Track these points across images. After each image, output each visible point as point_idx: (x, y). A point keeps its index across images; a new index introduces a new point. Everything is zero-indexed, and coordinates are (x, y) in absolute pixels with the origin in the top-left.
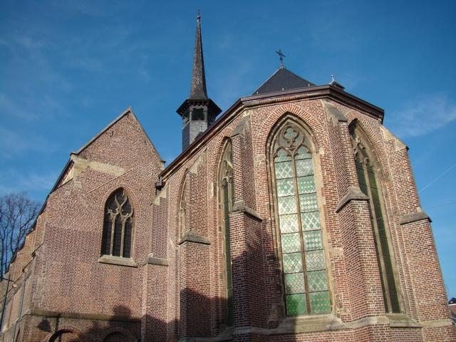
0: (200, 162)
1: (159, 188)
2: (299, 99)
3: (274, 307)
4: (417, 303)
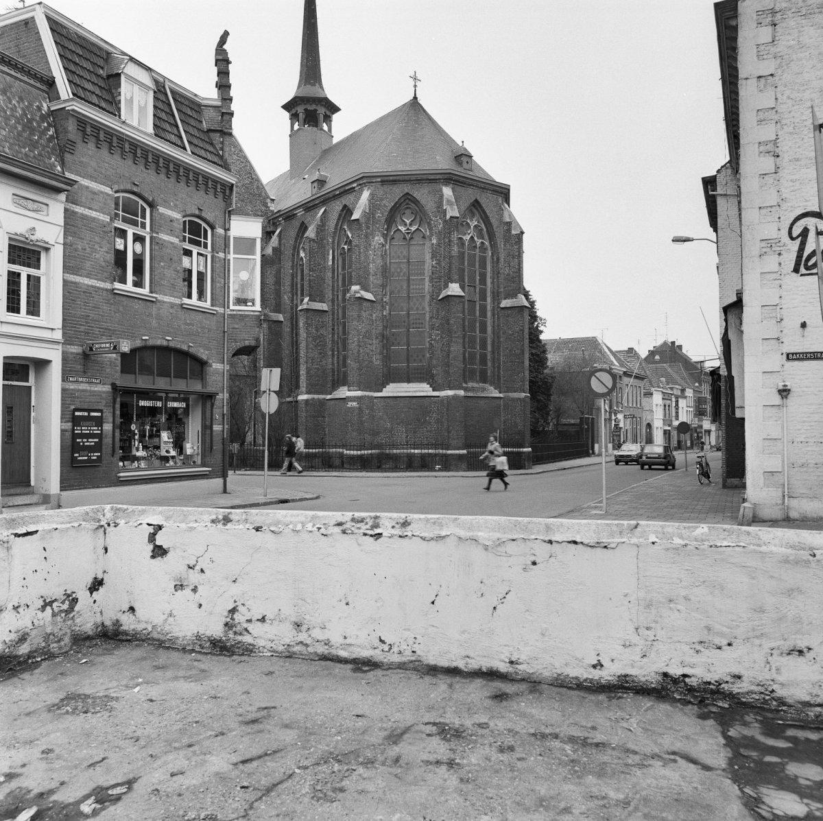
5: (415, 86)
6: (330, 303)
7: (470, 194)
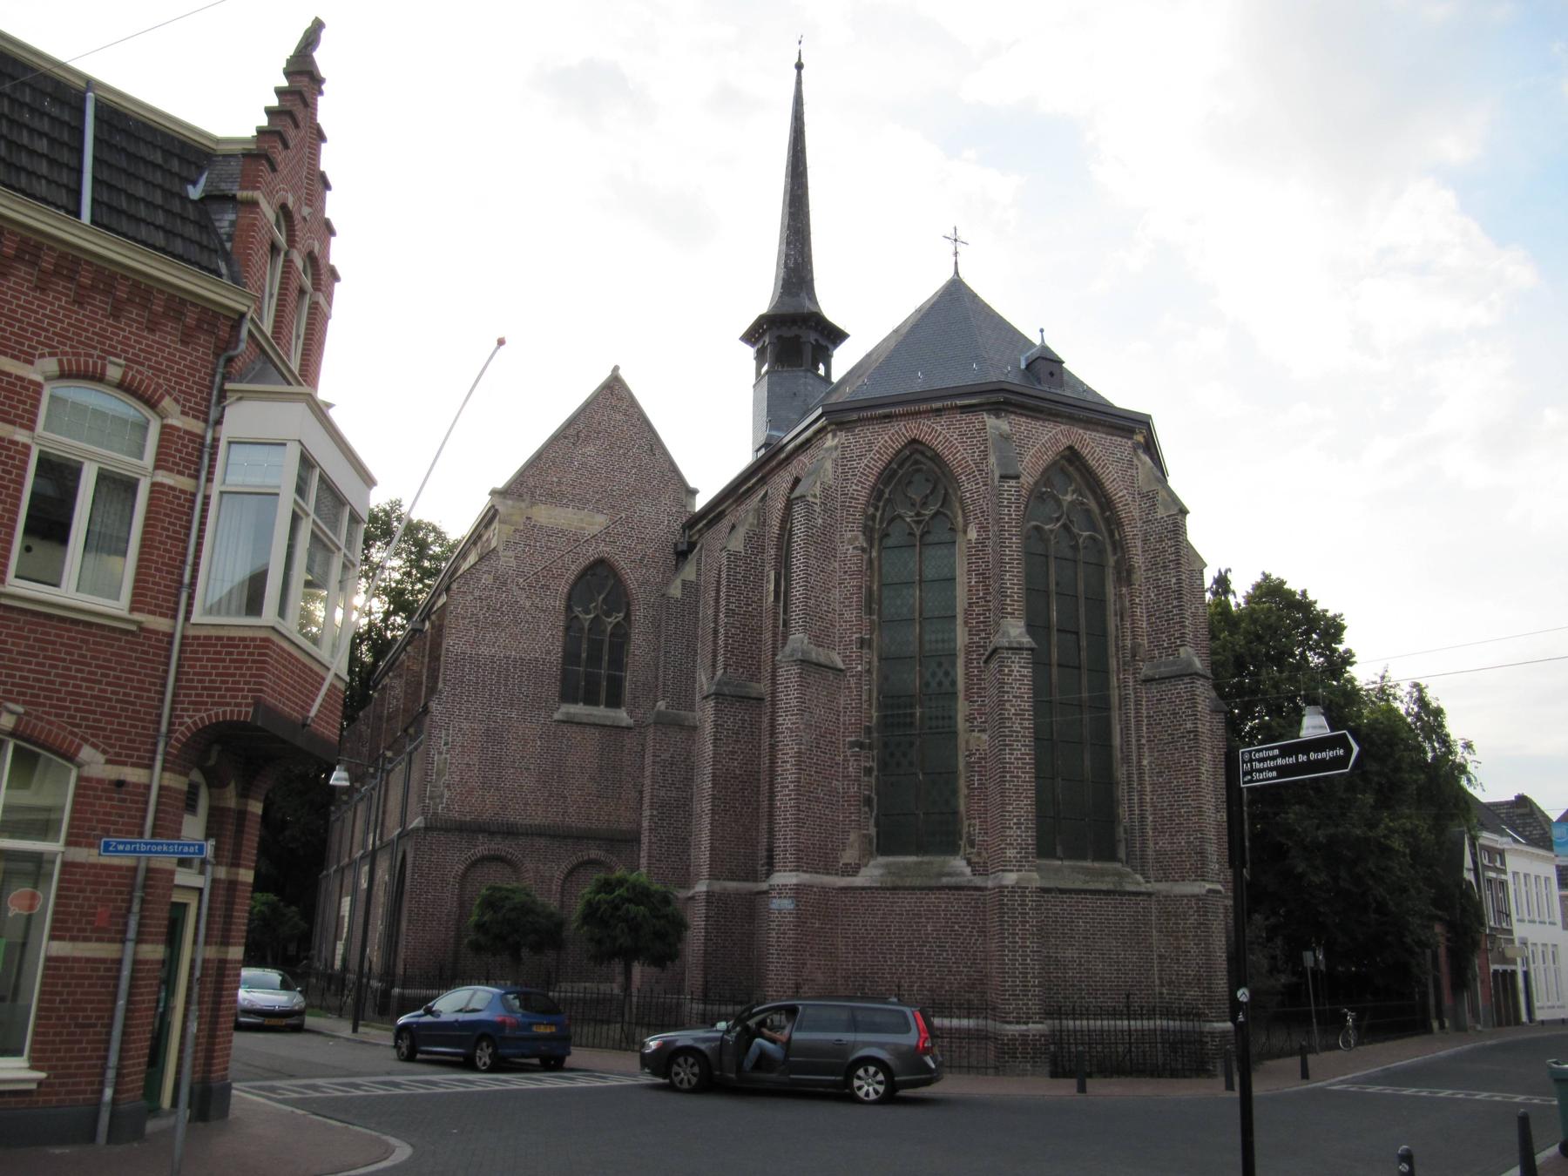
0: (751, 525)
1: (682, 555)
2: (938, 410)
3: (853, 837)
4: (1151, 844)
5: (956, 254)
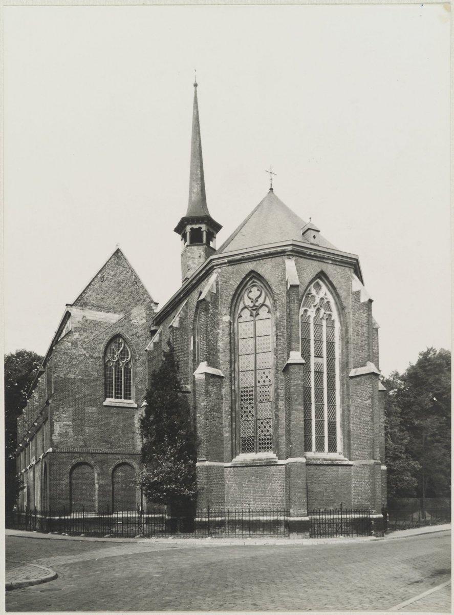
6: (192, 385)
7: (313, 268)
